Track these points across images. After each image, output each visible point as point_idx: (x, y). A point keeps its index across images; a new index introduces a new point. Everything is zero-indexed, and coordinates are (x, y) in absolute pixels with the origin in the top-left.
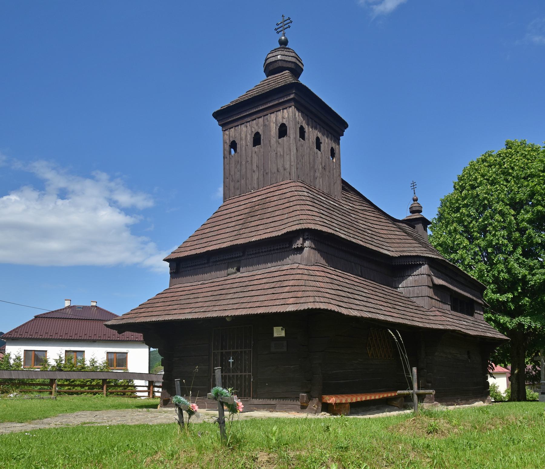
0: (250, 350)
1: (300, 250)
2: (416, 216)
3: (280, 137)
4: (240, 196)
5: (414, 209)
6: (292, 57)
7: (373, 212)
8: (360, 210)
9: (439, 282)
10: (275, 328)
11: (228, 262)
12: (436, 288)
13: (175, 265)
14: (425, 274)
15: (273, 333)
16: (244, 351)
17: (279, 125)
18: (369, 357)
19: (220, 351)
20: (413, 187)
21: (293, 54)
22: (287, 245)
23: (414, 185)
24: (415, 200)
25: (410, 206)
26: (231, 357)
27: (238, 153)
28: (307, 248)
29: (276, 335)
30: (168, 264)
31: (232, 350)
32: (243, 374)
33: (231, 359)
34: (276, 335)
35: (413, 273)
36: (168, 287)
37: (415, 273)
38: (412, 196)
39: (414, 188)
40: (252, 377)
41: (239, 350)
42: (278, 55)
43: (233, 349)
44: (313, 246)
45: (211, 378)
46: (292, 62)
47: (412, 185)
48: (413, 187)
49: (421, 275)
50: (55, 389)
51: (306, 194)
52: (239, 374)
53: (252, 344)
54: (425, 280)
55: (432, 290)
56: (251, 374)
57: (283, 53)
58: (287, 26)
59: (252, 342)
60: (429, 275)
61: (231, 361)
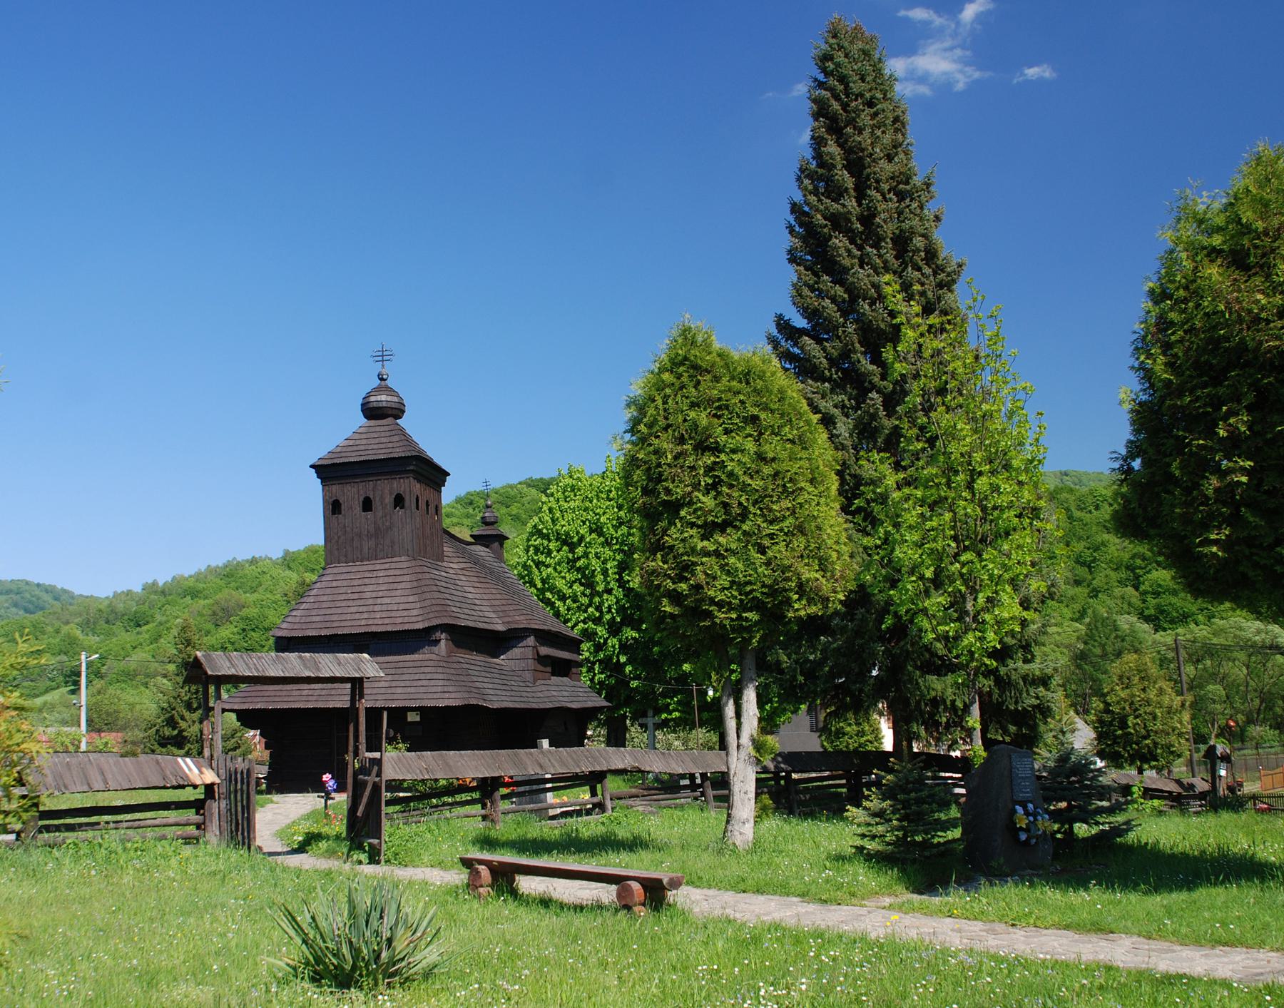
1: (437, 642)
9: (544, 651)
12: (542, 660)
29: (409, 720)
34: (409, 720)
54: (530, 653)
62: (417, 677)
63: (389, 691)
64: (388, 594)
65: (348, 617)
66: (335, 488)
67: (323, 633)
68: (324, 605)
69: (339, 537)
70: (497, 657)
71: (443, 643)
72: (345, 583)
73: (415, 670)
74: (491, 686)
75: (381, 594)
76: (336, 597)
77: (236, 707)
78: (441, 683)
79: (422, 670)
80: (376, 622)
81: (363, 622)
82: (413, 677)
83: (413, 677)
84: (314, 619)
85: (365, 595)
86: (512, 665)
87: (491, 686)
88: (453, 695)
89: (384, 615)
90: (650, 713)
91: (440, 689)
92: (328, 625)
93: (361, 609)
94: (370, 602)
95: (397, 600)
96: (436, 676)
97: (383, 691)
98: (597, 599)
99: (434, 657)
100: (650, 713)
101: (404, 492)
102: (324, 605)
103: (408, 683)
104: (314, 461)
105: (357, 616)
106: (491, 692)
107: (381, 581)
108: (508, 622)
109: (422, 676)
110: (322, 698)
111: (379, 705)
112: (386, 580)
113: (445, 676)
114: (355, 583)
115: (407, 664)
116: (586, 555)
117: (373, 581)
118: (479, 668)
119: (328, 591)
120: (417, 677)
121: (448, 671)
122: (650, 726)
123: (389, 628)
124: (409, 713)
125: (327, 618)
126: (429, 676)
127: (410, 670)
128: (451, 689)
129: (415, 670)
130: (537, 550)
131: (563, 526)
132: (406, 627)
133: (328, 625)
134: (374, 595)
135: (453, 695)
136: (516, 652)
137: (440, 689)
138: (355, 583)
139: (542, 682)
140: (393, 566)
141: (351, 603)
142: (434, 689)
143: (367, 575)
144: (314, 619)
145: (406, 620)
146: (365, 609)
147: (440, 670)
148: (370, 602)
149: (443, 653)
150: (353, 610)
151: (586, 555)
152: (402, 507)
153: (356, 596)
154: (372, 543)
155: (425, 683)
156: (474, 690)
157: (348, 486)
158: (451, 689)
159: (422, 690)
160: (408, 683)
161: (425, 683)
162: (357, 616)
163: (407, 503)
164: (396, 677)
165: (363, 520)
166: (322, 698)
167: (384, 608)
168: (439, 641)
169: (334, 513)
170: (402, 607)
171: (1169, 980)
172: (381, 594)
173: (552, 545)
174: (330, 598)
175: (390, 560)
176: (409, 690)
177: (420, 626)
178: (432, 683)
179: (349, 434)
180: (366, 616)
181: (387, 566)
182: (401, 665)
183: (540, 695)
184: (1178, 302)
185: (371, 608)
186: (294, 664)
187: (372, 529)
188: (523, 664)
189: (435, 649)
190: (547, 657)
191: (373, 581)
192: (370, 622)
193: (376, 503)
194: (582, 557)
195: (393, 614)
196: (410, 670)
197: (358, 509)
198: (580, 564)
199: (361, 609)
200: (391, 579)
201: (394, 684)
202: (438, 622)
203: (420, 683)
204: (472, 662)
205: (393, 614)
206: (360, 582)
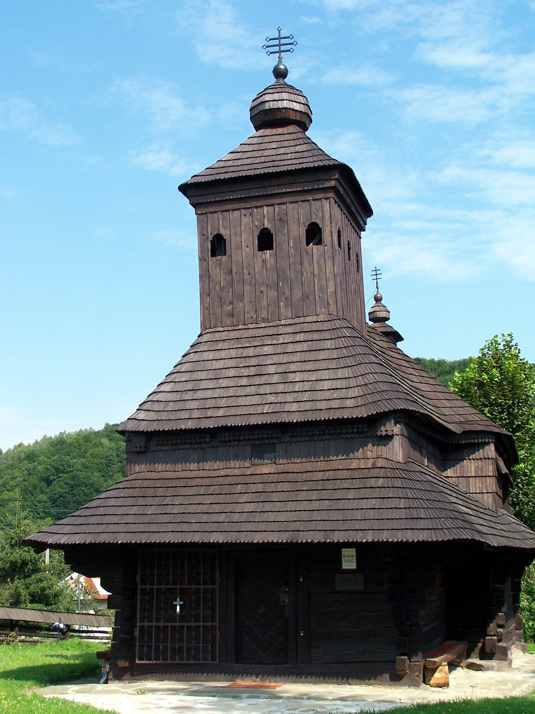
1: (389, 438)
3: (307, 246)
10: (354, 549)
20: (375, 277)
39: (377, 279)
48: (375, 277)
60: (495, 460)
68: (204, 385)
75: (293, 367)
77: (63, 540)
91: (402, 514)
102: (204, 385)
104: (186, 179)
111: (338, 537)
149: (400, 457)
152: (320, 242)
153: (253, 371)
163: (326, 236)
168: (392, 436)
169: (214, 254)
171: (219, 614)
177: (363, 413)
179: (235, 146)
184: (524, 371)
186: (341, 254)
202: (401, 405)
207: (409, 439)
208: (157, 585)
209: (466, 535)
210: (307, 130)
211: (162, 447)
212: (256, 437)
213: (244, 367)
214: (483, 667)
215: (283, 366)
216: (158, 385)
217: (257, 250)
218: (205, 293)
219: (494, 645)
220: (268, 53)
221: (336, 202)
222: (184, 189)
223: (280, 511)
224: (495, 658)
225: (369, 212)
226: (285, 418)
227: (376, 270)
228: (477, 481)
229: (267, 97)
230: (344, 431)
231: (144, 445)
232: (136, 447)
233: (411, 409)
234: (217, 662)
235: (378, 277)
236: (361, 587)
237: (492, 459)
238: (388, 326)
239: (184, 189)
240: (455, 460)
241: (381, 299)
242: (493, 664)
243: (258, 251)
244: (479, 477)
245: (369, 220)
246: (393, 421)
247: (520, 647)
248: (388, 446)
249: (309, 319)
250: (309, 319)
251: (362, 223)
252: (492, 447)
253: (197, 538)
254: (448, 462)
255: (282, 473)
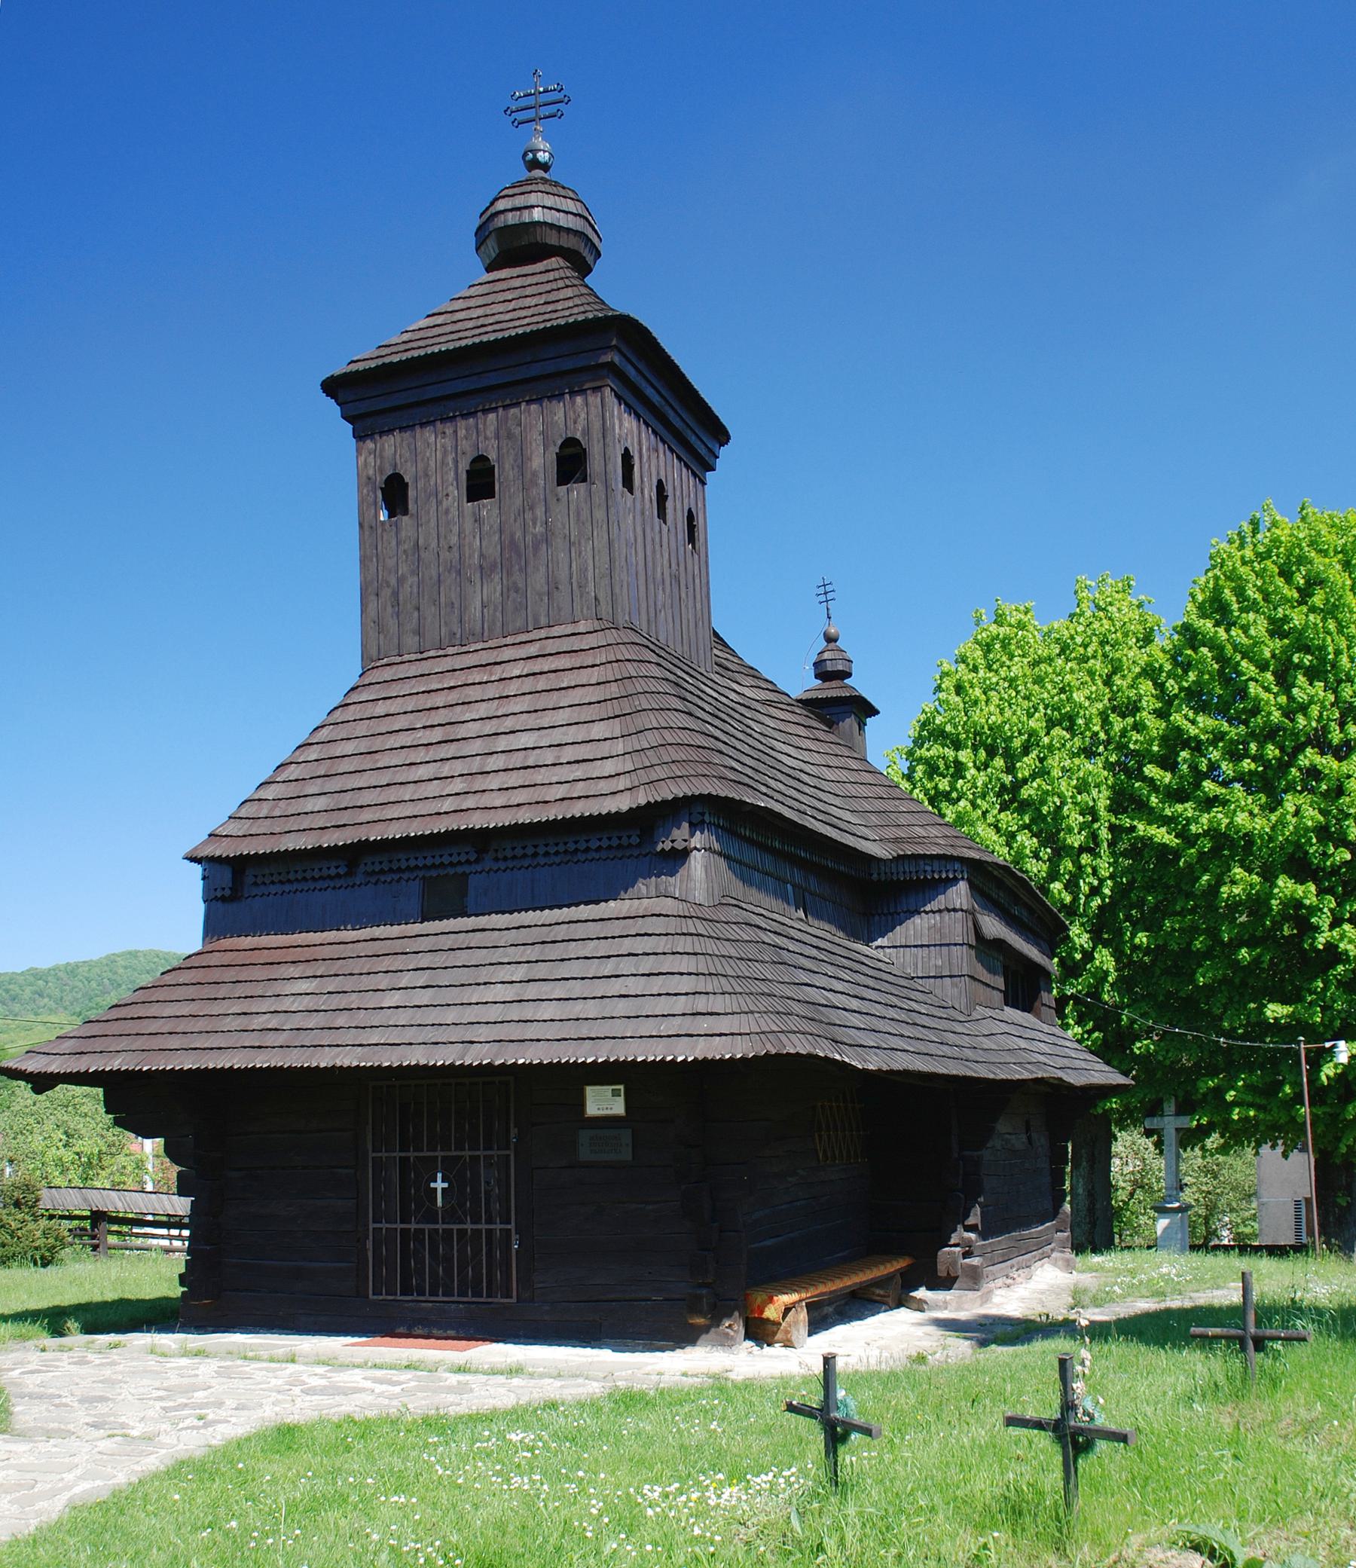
0: (507, 1152)
1: (680, 856)
2: (833, 690)
4: (425, 655)
5: (830, 667)
6: (575, 215)
7: (789, 708)
8: (758, 701)
9: (993, 927)
10: (100, 1091)
11: (424, 878)
12: (987, 948)
13: (226, 875)
14: (962, 910)
15: (582, 1105)
16: (485, 1156)
17: (559, 442)
18: (819, 1160)
19: (397, 1154)
20: (822, 598)
21: (570, 206)
22: (634, 840)
23: (826, 592)
24: (830, 639)
25: (814, 658)
26: (439, 1175)
27: (412, 515)
28: (699, 850)
29: (593, 1109)
30: (197, 870)
31: (440, 1154)
32: (483, 1226)
33: (439, 1179)
34: (593, 1109)
35: (925, 905)
36: (198, 946)
37: (928, 908)
38: (821, 625)
39: (827, 601)
40: (514, 1237)
41: (467, 1153)
42: (533, 207)
43: (446, 1147)
44: (716, 846)
45: (367, 1238)
46: (576, 233)
47: (822, 590)
48: (822, 598)
49: (949, 910)
50: (1187, 1524)
51: (656, 671)
52: (469, 1226)
53: (512, 1135)
54: (957, 928)
55: (973, 953)
56: (512, 1226)
57: (549, 201)
58: (553, 109)
59: (514, 1131)
60: (970, 912)
61: (439, 1185)
62: (608, 967)
63: (515, 1012)
64: (531, 721)
65: (407, 793)
66: (390, 444)
67: (328, 840)
69: (401, 581)
70: (868, 941)
71: (697, 862)
72: (411, 704)
73: (604, 947)
74: (855, 1004)
75: (509, 724)
76: (378, 744)
78: (686, 984)
79: (627, 945)
80: (486, 800)
81: (448, 805)
82: (593, 968)
83: (593, 968)
84: (310, 805)
85: (462, 731)
86: (906, 962)
87: (855, 1004)
88: (724, 1025)
89: (514, 779)
90: (1170, 1107)
91: (680, 1005)
92: (345, 818)
93: (446, 769)
94: (477, 746)
95: (557, 736)
96: (668, 964)
97: (494, 1013)
98: (1067, 865)
99: (668, 905)
100: (1170, 1107)
101: (587, 431)
103: (576, 989)
104: (340, 368)
105: (433, 789)
106: (855, 1020)
107: (512, 688)
108: (896, 840)
109: (626, 966)
110: (307, 1039)
112: (528, 685)
113: (701, 965)
114: (439, 700)
115: (580, 931)
116: (1042, 772)
117: (492, 691)
118: (814, 952)
119: (362, 729)
120: (608, 967)
121: (710, 946)
122: (1170, 1137)
123: (525, 816)
124: (590, 1091)
125: (346, 800)
126: (647, 965)
127: (589, 949)
128: (718, 1004)
129: (604, 947)
130: (932, 770)
131: (987, 715)
132: (578, 810)
133: (345, 818)
134: (489, 727)
135: (724, 1025)
136: (917, 927)
137: (680, 1005)
138: (439, 700)
139: (989, 1012)
140: (551, 646)
141: (420, 755)
142: (662, 1006)
143: (476, 676)
144: (310, 805)
145: (579, 789)
146: (459, 767)
147: (683, 944)
148: (477, 746)
150: (423, 772)
151: (1042, 772)
153: (437, 735)
154: (493, 589)
155: (633, 986)
156: (797, 1008)
157: (428, 434)
158: (718, 1004)
159: (622, 1007)
160: (576, 989)
161: (633, 986)
162: (433, 789)
163: (595, 464)
164: (541, 970)
165: (469, 524)
166: (307, 1039)
167: (517, 760)
170: (569, 754)
172: (509, 724)
173: (965, 756)
174: (363, 746)
175: (543, 633)
176: (577, 1009)
177: (623, 804)
178: (657, 985)
180: (458, 785)
181: (533, 649)
182: (561, 932)
183: (987, 1043)
185: (475, 765)
187: (493, 551)
188: (936, 960)
189: (673, 883)
190: (999, 944)
191: (492, 691)
192: (470, 802)
193: (505, 475)
194: (1034, 776)
195: (540, 776)
196: (589, 949)
197: (455, 491)
198: (1025, 793)
199: (446, 769)
200: (542, 683)
201: (532, 991)
202: (681, 789)
203: (616, 987)
204: (793, 933)
205: (540, 776)
206: (453, 697)
207: (727, 857)
208: (485, 1149)
209: (823, 1050)
210: (590, 270)
211: (262, 887)
212: (429, 862)
213: (424, 727)
214: (926, 1303)
215: (495, 721)
216: (278, 767)
217: (465, 500)
218: (369, 591)
219: (954, 1263)
220: (516, 124)
221: (617, 396)
222: (332, 387)
223: (449, 1005)
224: (955, 1286)
225: (721, 434)
226: (478, 821)
227: (824, 585)
228: (933, 955)
229: (501, 205)
230: (594, 844)
231: (230, 885)
232: (223, 889)
233: (723, 794)
234: (514, 1300)
235: (830, 596)
236: (626, 1155)
237: (962, 910)
238: (847, 687)
239: (332, 387)
240: (891, 914)
241: (836, 640)
242: (948, 1298)
243: (468, 502)
244: (935, 945)
245: (723, 451)
246: (685, 825)
247: (1060, 1263)
248: (678, 875)
249: (557, 631)
250: (557, 631)
251: (703, 451)
252: (963, 886)
253: (237, 1061)
254: (877, 918)
255: (473, 931)
